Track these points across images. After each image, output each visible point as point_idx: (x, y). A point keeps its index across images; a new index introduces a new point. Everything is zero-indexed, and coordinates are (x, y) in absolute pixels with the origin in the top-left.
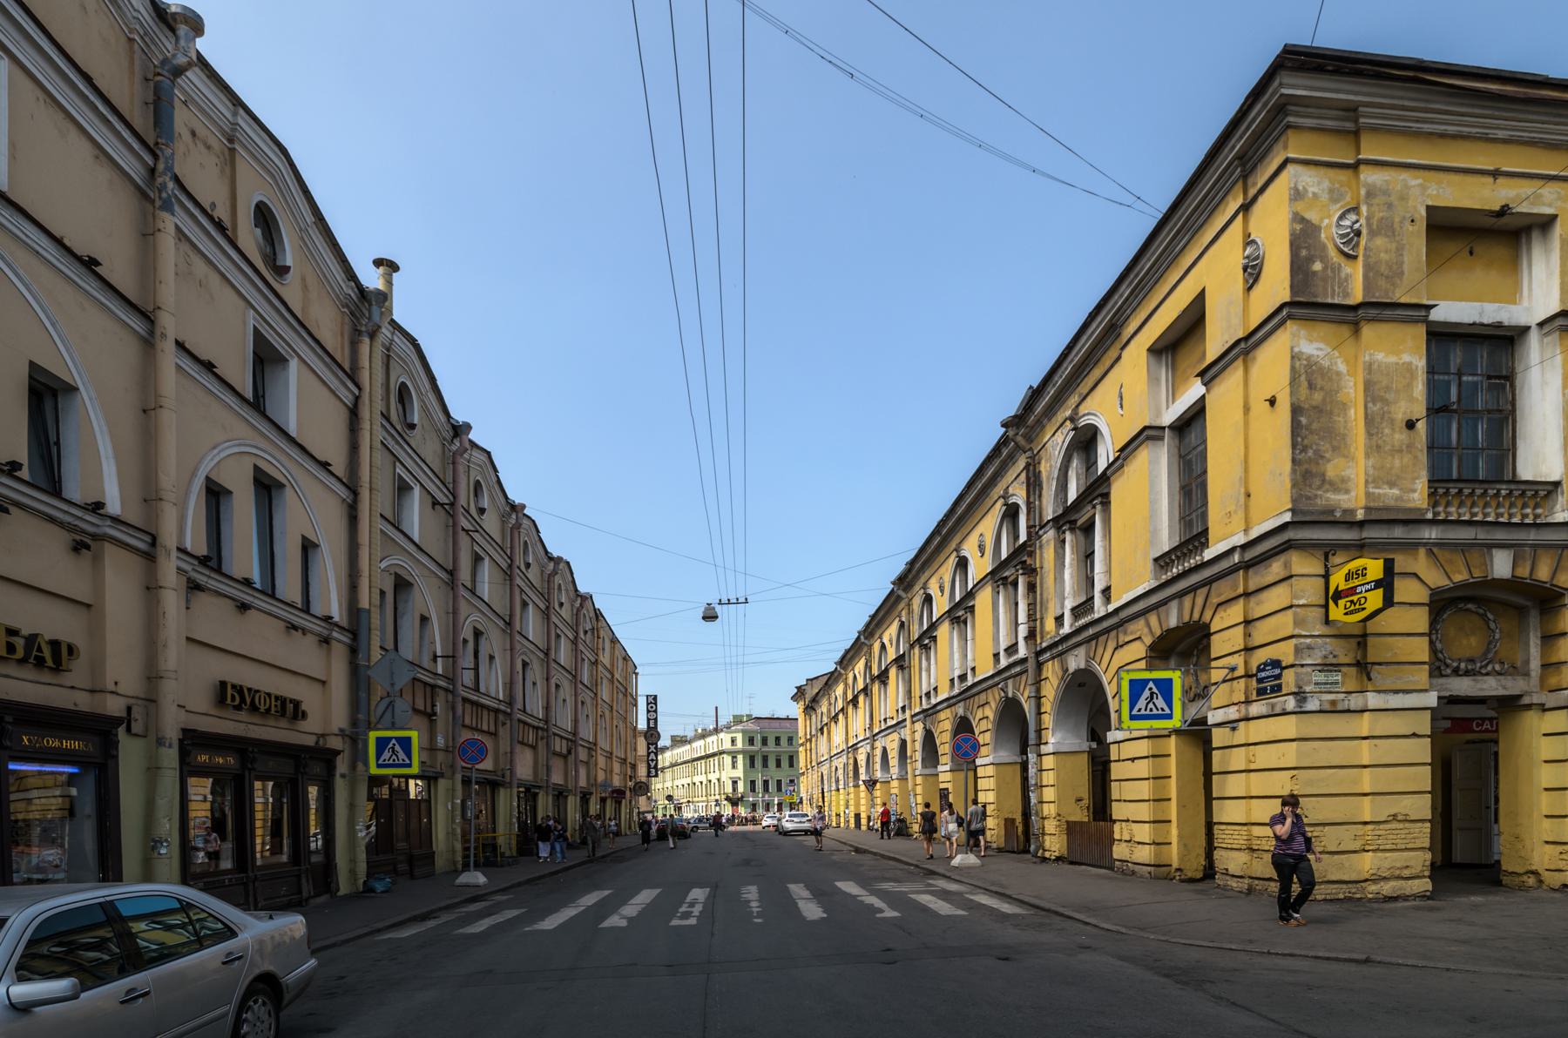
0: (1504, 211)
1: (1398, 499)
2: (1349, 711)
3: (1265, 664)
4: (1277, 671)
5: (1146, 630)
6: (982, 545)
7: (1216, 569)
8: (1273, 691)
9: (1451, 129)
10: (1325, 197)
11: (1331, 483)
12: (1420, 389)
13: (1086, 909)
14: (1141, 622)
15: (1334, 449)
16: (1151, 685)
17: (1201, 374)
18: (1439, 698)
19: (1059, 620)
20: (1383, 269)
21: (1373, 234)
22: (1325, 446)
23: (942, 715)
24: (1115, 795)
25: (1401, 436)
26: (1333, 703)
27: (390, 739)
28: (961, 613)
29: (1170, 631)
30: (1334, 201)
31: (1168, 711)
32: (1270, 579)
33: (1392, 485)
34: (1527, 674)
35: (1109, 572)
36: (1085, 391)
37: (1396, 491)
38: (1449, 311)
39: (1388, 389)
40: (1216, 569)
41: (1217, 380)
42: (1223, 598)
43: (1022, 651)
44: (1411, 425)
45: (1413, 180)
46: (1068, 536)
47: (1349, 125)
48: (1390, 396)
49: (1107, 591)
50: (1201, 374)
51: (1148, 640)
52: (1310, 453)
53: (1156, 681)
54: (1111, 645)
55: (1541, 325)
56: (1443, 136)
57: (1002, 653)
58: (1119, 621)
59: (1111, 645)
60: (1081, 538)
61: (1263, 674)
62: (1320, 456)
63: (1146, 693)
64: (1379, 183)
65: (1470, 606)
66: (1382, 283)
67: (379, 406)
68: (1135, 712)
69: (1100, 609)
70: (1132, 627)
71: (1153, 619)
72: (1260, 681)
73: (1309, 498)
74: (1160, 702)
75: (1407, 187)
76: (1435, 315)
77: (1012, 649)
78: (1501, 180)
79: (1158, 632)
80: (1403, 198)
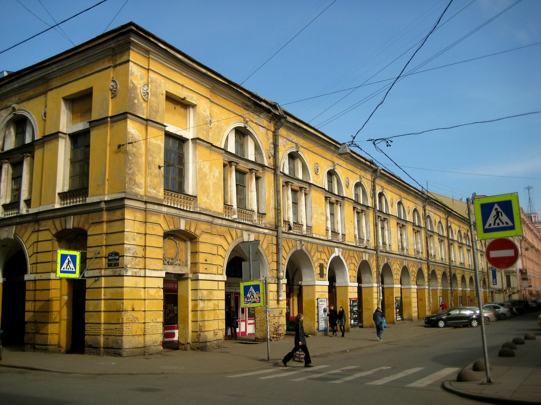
0: (184, 99)
2: (140, 276)
3: (112, 253)
4: (117, 257)
5: (53, 226)
8: (115, 265)
10: (139, 77)
11: (137, 185)
13: (23, 373)
14: (50, 222)
15: (139, 171)
18: (166, 273)
20: (154, 109)
21: (152, 95)
22: (135, 169)
25: (157, 171)
26: (136, 273)
27: (249, 286)
29: (66, 229)
30: (142, 79)
32: (116, 218)
33: (154, 189)
34: (187, 266)
37: (155, 191)
38: (171, 129)
39: (154, 152)
41: (97, 127)
42: (94, 221)
44: (160, 167)
45: (162, 80)
48: (154, 155)
49: (28, 202)
52: (131, 171)
55: (192, 139)
56: (170, 68)
60: (13, 169)
61: (111, 258)
62: (134, 173)
66: (154, 113)
67: (294, 301)
70: (43, 223)
71: (57, 222)
72: (109, 260)
73: (130, 189)
76: (167, 129)
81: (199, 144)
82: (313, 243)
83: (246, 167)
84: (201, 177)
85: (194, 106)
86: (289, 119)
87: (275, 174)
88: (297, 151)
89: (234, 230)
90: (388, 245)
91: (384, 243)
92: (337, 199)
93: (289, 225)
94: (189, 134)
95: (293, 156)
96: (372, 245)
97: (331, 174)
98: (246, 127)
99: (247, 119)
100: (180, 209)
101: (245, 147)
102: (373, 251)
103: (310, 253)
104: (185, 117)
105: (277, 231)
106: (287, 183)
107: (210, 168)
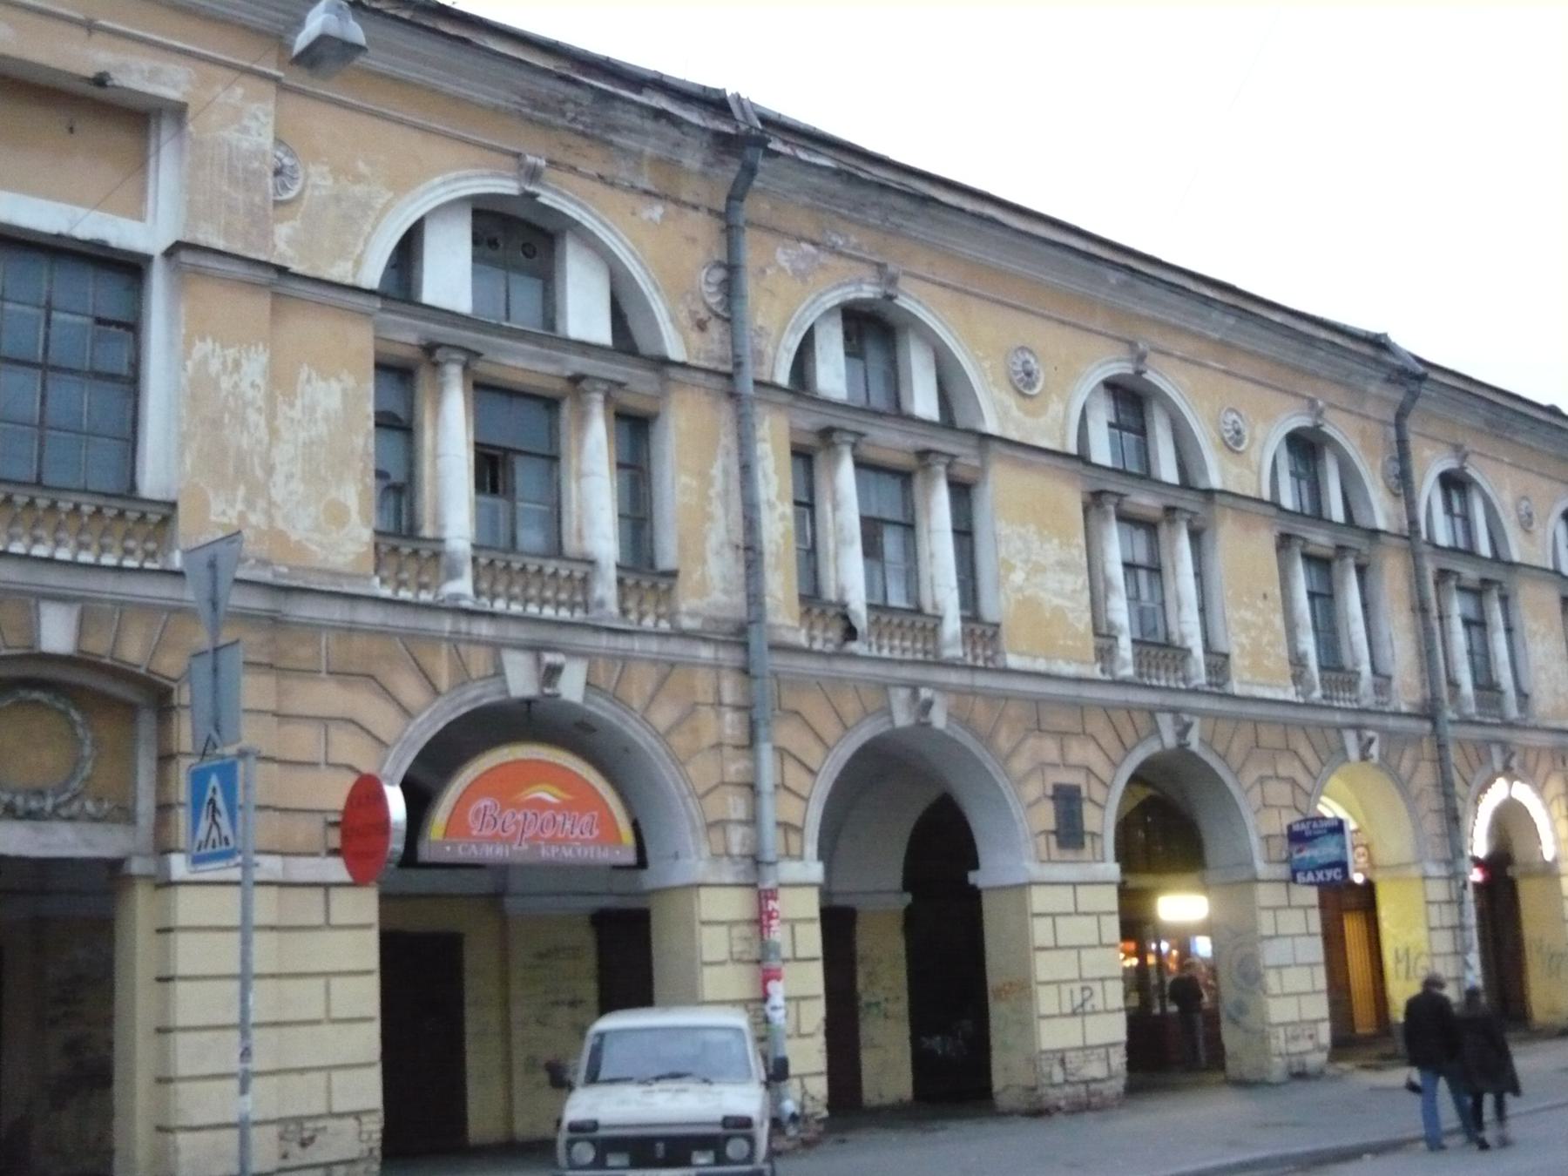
0: (101, 81)
81: (198, 272)
82: (1006, 697)
83: (551, 369)
84: (206, 409)
85: (178, 112)
86: (1433, 375)
87: (1416, 556)
88: (890, 298)
89: (444, 647)
90: (1511, 694)
91: (1487, 686)
92: (1172, 502)
93: (845, 617)
94: (143, 235)
95: (1454, 483)
96: (1407, 690)
97: (1306, 448)
98: (533, 196)
99: (530, 159)
100: (1168, 689)
101: (558, 297)
102: (1411, 724)
103: (988, 740)
104: (140, 164)
105: (745, 646)
106: (1443, 575)
107: (280, 381)
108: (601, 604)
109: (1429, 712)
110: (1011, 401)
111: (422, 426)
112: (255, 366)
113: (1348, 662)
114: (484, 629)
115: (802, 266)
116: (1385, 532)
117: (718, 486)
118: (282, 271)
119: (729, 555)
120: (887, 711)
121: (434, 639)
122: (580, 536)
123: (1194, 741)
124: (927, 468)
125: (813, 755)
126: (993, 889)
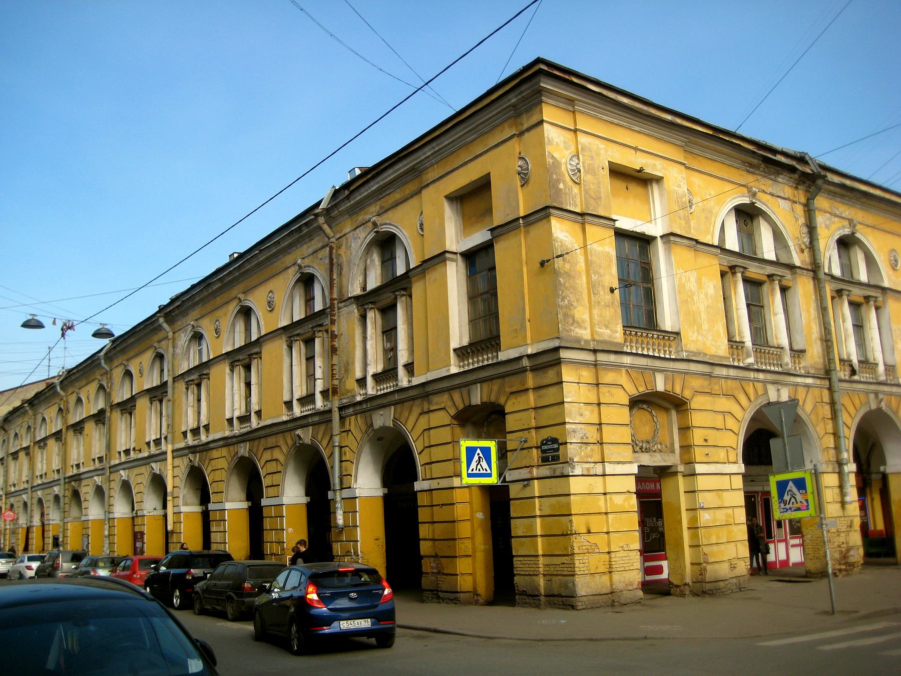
1: (610, 336)
3: (547, 440)
4: (556, 446)
5: (450, 403)
6: (278, 303)
7: (509, 368)
8: (553, 460)
9: (616, 121)
10: (562, 145)
12: (614, 270)
14: (446, 396)
15: (578, 300)
16: (479, 451)
17: (492, 230)
19: (362, 382)
21: (586, 172)
22: (572, 298)
23: (215, 454)
24: (212, 540)
25: (608, 296)
26: (588, 469)
28: (244, 358)
31: (489, 471)
33: (607, 327)
35: (411, 351)
36: (387, 206)
37: (608, 331)
39: (600, 266)
40: (509, 368)
42: (514, 389)
43: (319, 403)
44: (612, 290)
46: (370, 315)
47: (571, 108)
48: (601, 271)
50: (492, 230)
51: (453, 412)
53: (482, 449)
54: (416, 411)
55: (661, 237)
57: (295, 402)
58: (425, 393)
59: (416, 411)
61: (546, 447)
63: (476, 458)
64: (586, 144)
65: (645, 406)
68: (470, 471)
69: (403, 380)
70: (435, 399)
71: (456, 396)
72: (544, 452)
73: (567, 331)
74: (484, 464)
75: (598, 148)
76: (618, 225)
77: (307, 399)
78: (639, 153)
79: (461, 407)
80: (598, 155)
81: (675, 243)
83: (762, 272)
84: (683, 299)
85: (659, 180)
89: (751, 384)
93: (851, 366)
94: (655, 229)
95: (845, 244)
99: (754, 189)
104: (647, 200)
105: (830, 379)
106: (839, 293)
107: (699, 281)
108: (787, 364)
109: (827, 373)
110: (891, 272)
111: (731, 296)
112: (693, 276)
113: (773, 341)
114: (761, 376)
115: (828, 223)
116: (799, 268)
117: (813, 316)
118: (697, 241)
119: (819, 343)
120: (868, 403)
121: (748, 380)
122: (777, 338)
123: (883, 405)
124: (868, 302)
125: (739, 413)
126: (892, 473)
